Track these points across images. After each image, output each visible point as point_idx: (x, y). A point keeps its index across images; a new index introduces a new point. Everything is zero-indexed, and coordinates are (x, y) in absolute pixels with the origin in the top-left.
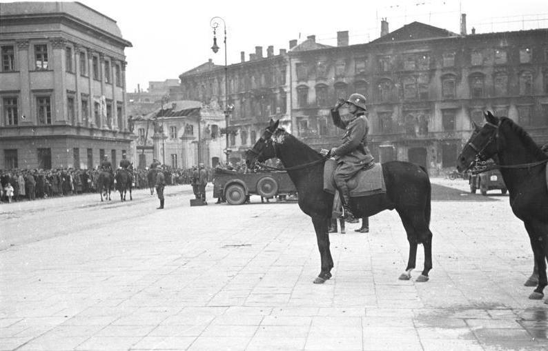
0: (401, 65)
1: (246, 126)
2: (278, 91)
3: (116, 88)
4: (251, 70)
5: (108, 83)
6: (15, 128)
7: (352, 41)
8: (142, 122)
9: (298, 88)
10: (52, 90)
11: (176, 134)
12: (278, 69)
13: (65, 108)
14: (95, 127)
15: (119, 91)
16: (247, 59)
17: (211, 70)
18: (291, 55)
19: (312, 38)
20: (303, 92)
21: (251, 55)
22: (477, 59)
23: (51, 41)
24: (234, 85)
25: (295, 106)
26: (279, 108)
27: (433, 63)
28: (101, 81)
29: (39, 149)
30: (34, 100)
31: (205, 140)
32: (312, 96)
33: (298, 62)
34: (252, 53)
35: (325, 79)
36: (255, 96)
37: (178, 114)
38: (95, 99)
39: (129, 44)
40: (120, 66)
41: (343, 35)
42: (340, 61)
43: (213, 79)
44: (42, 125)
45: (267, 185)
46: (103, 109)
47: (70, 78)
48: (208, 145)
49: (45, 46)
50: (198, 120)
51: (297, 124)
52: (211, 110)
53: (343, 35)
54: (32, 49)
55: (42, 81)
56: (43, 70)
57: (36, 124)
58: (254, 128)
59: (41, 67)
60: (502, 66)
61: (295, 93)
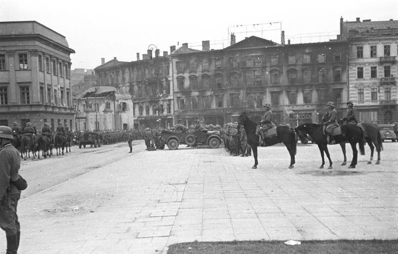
0: (245, 64)
1: (143, 103)
2: (164, 80)
3: (53, 76)
4: (145, 65)
5: (61, 77)
6: (5, 106)
9: (177, 78)
10: (30, 82)
11: (98, 109)
12: (164, 65)
13: (39, 94)
14: (55, 105)
15: (67, 81)
16: (141, 58)
17: (117, 65)
18: (173, 56)
19: (186, 45)
20: (181, 80)
21: (144, 55)
22: (292, 60)
23: (30, 52)
25: (176, 90)
26: (165, 91)
27: (265, 63)
28: (57, 76)
29: (22, 120)
30: (19, 90)
31: (118, 112)
33: (177, 61)
34: (145, 54)
35: (196, 72)
36: (149, 83)
37: (100, 95)
39: (73, 52)
41: (206, 44)
42: (205, 60)
43: (119, 71)
44: (24, 104)
45: (190, 139)
47: (41, 74)
48: (121, 116)
49: (26, 55)
52: (122, 93)
53: (206, 44)
54: (17, 57)
55: (24, 77)
56: (24, 70)
57: (20, 104)
59: (22, 67)
60: (308, 65)
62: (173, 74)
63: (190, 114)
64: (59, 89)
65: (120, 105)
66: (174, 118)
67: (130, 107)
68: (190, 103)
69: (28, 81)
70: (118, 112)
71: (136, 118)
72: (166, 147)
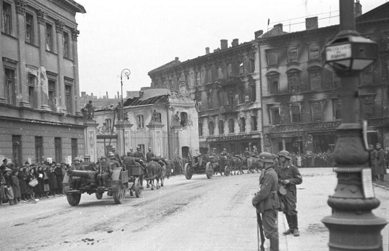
1: (214, 116)
2: (246, 80)
7: (322, 24)
8: (109, 112)
9: (267, 75)
11: (143, 123)
12: (246, 57)
20: (273, 79)
24: (201, 78)
25: (266, 93)
26: (247, 97)
31: (173, 128)
32: (283, 83)
33: (268, 48)
35: (297, 64)
37: (145, 102)
38: (28, 70)
39: (81, 9)
40: (70, 34)
46: (43, 85)
48: (177, 133)
50: (167, 107)
51: (268, 112)
52: (179, 96)
58: (222, 118)
61: (264, 80)
62: (260, 70)
63: (287, 131)
64: (42, 76)
65: (176, 116)
66: (262, 137)
67: (193, 120)
68: (289, 113)
70: (173, 128)
71: (205, 140)
72: (77, 35)
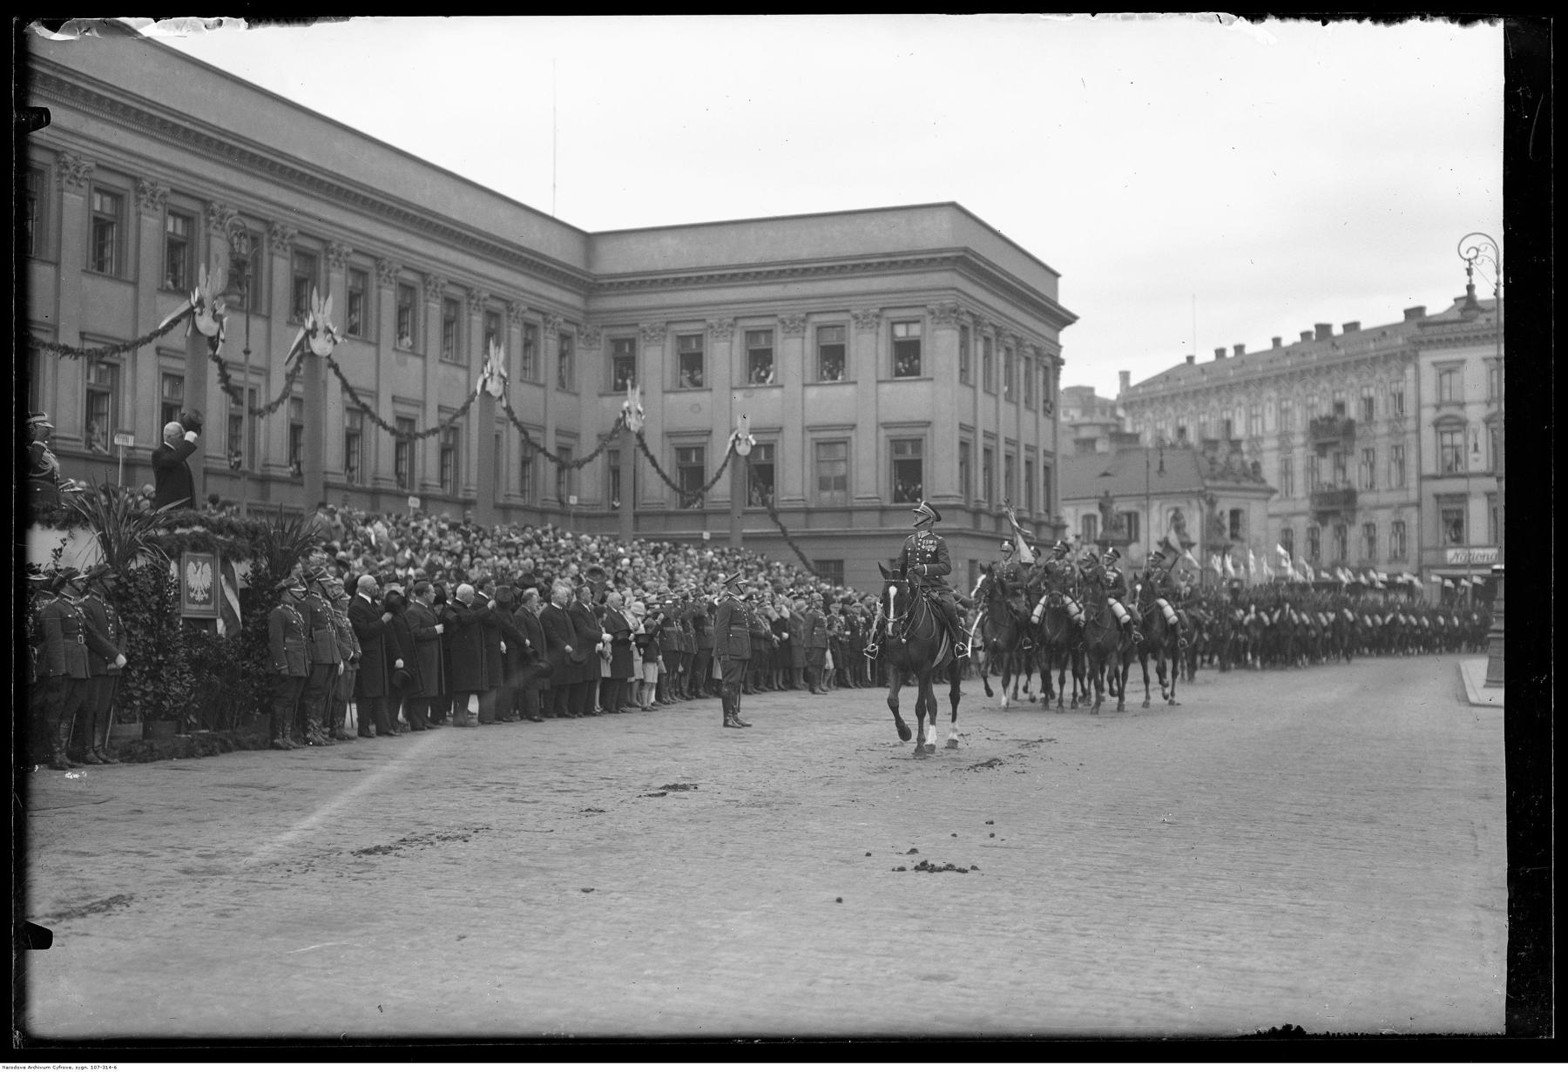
10: (928, 424)
69: (840, 420)
